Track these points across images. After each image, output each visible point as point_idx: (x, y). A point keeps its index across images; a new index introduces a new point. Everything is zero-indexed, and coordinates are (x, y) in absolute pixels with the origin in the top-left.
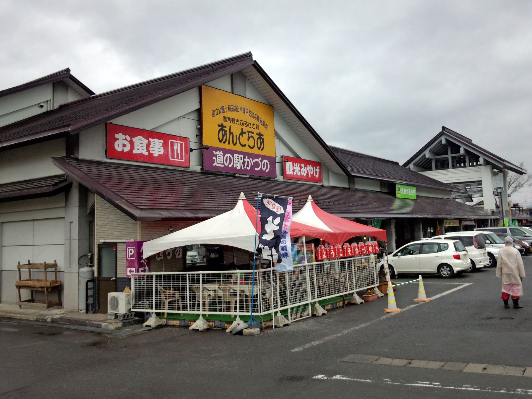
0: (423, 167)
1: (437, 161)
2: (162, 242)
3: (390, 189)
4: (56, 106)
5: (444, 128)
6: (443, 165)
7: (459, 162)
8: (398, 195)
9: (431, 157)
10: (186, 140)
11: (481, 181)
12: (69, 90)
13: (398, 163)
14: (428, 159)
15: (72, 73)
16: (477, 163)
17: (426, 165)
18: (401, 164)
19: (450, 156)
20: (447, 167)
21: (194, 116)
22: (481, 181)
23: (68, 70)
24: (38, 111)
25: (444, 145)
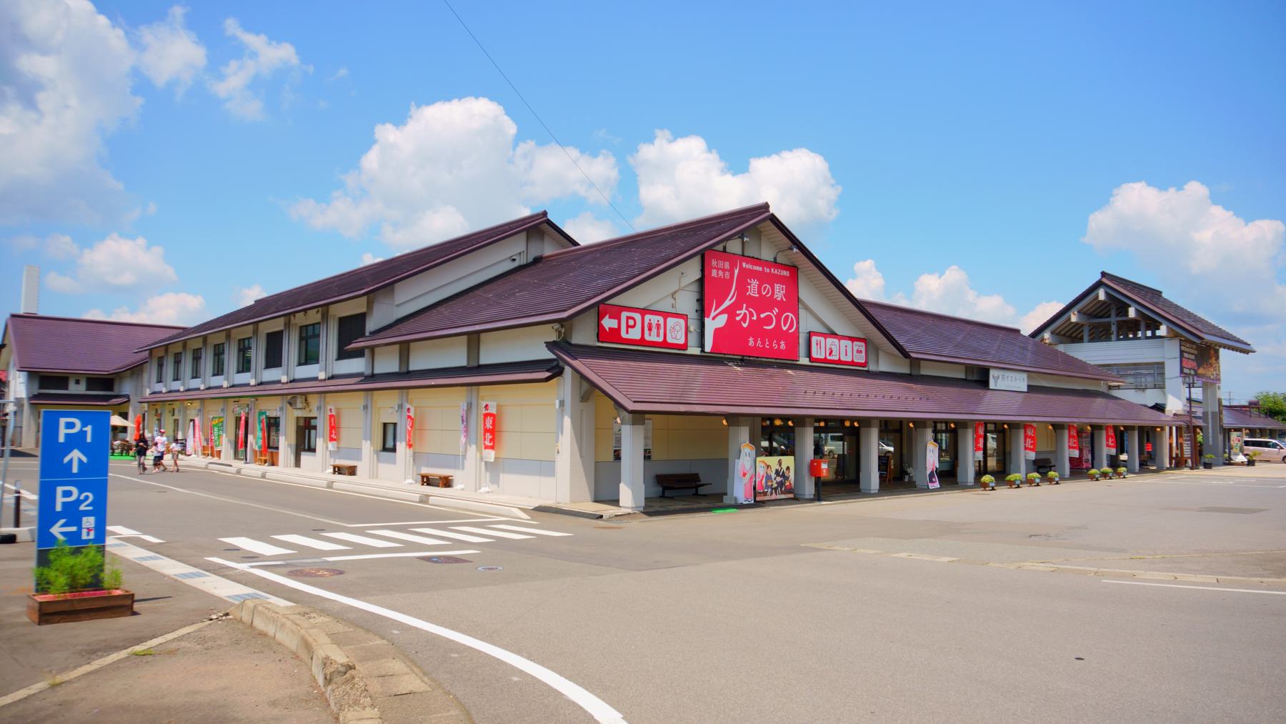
0: (1070, 336)
1: (1093, 328)
2: (112, 691)
3: (980, 378)
4: (530, 260)
5: (1104, 274)
6: (1101, 334)
7: (1129, 329)
8: (992, 385)
9: (1082, 322)
10: (684, 317)
11: (1162, 364)
12: (546, 238)
13: (1017, 331)
14: (1077, 324)
15: (550, 217)
16: (1153, 333)
17: (1072, 335)
18: (1027, 330)
19: (1114, 319)
20: (1108, 339)
21: (695, 288)
22: (1162, 364)
23: (545, 214)
24: (509, 266)
25: (1103, 303)
